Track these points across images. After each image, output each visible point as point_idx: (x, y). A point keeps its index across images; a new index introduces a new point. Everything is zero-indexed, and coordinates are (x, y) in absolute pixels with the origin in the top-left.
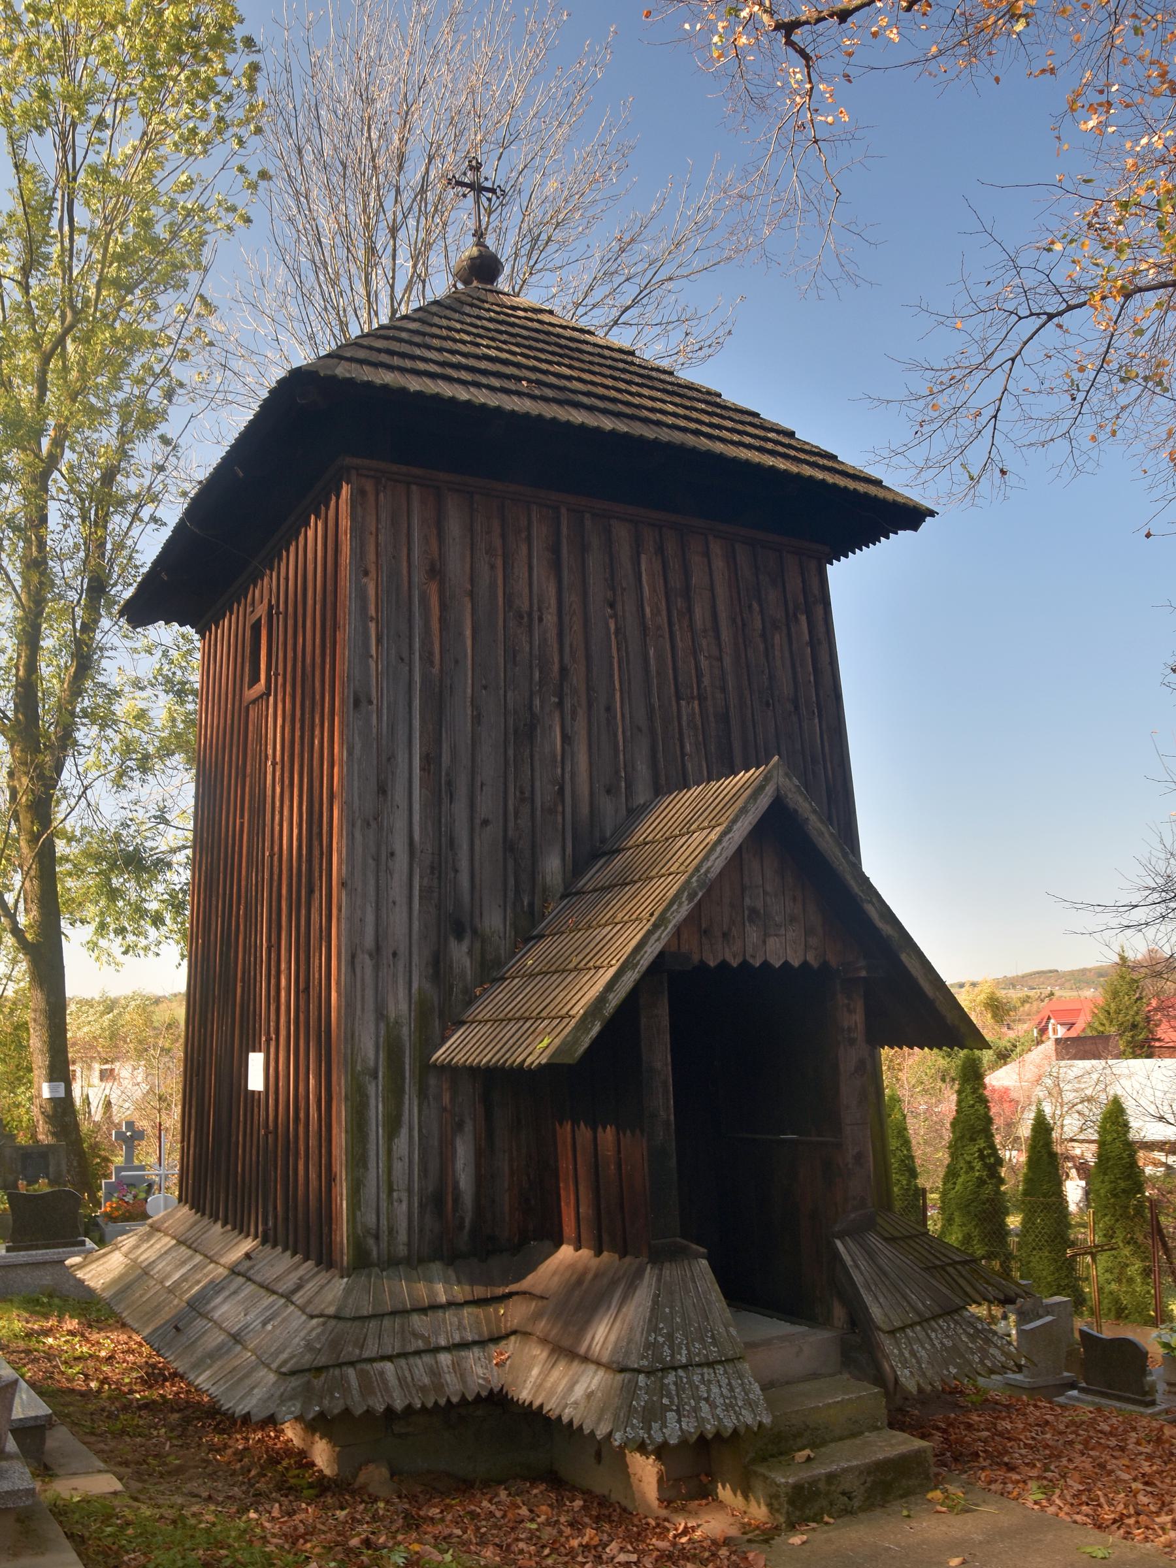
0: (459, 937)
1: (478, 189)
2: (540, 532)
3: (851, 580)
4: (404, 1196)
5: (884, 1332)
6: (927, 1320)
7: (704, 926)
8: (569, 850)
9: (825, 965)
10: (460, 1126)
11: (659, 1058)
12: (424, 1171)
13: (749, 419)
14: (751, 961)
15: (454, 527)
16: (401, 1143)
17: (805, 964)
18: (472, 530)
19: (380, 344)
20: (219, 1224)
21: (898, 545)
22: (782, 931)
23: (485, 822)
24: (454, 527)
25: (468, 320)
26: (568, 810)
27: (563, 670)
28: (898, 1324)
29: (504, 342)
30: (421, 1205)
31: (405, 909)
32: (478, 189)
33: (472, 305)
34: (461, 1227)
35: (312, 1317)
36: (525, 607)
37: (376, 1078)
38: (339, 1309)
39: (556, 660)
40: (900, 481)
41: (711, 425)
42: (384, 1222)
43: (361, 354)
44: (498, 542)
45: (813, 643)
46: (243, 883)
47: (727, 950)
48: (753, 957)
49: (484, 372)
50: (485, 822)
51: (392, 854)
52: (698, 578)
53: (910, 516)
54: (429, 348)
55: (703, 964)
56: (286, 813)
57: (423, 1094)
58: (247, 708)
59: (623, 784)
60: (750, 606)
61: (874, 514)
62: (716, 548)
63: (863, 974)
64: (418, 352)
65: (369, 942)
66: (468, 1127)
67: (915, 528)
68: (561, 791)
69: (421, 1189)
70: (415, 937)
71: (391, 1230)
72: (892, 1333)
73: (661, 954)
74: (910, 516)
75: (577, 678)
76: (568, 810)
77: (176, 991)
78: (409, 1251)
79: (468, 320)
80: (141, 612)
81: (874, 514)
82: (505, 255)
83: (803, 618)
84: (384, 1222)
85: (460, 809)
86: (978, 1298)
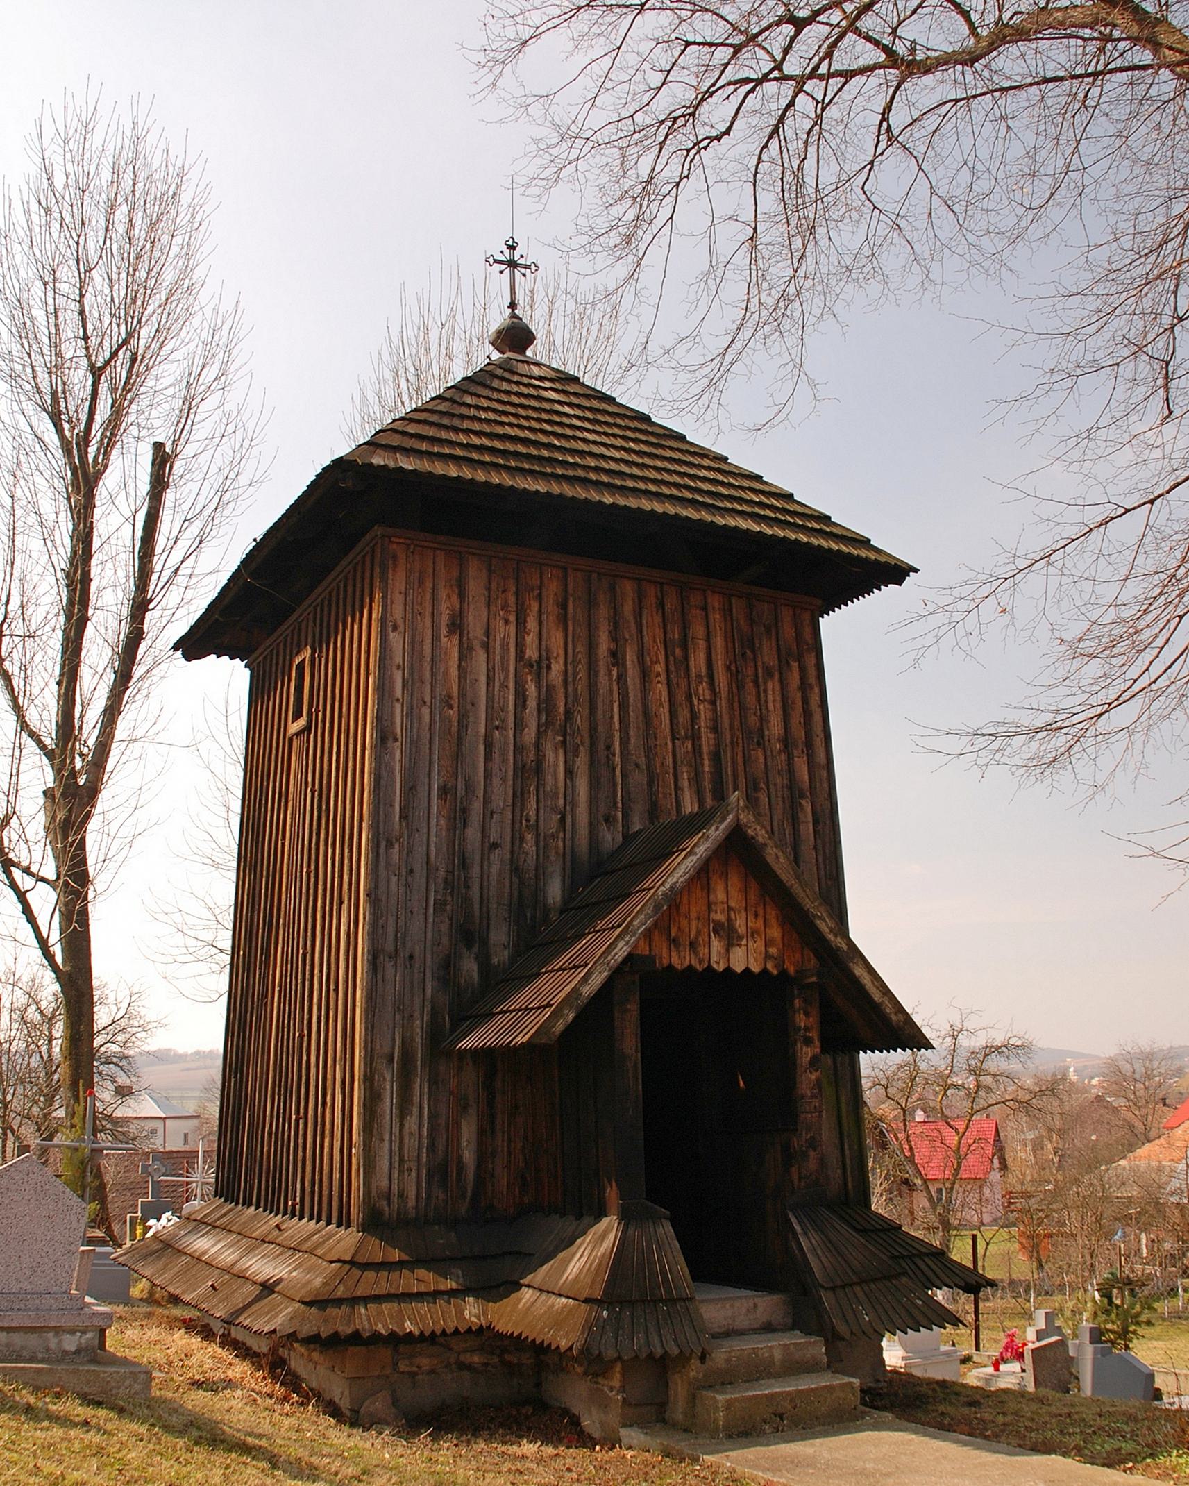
0: (469, 946)
1: (512, 264)
2: (552, 588)
3: (842, 630)
4: (413, 1165)
5: (826, 1289)
6: (865, 1282)
7: (673, 935)
8: (568, 872)
9: (783, 973)
10: (465, 1108)
11: (629, 1043)
12: (432, 1147)
13: (746, 483)
14: (715, 966)
15: (475, 587)
16: (411, 1123)
17: (765, 971)
18: (489, 589)
19: (412, 429)
20: (253, 1208)
21: (882, 601)
22: (744, 942)
23: (495, 846)
24: (475, 587)
25: (495, 396)
26: (568, 835)
27: (568, 713)
28: (839, 1283)
29: (527, 418)
30: (428, 1175)
31: (422, 917)
32: (512, 264)
33: (503, 379)
34: (464, 1195)
35: (331, 1262)
36: (535, 657)
37: (391, 1060)
38: (353, 1256)
39: (562, 704)
40: (889, 541)
41: (709, 493)
42: (395, 1187)
43: (396, 440)
44: (512, 600)
45: (804, 687)
46: (283, 897)
47: (674, 954)
48: (718, 963)
49: (504, 453)
50: (495, 846)
51: (412, 871)
52: (698, 630)
53: (896, 572)
54: (457, 430)
55: (670, 967)
56: (322, 836)
57: (434, 1081)
58: (291, 740)
59: (620, 814)
60: (744, 655)
61: (863, 571)
62: (715, 602)
63: (814, 979)
64: (444, 435)
65: (390, 947)
66: (472, 1111)
67: (899, 582)
68: (563, 820)
69: (429, 1161)
70: (429, 943)
71: (401, 1195)
72: (833, 1289)
73: (629, 958)
74: (896, 572)
75: (580, 721)
76: (568, 835)
77: (206, 1048)
78: (417, 1213)
79: (495, 396)
80: (194, 645)
81: (863, 571)
82: (538, 329)
83: (795, 665)
84: (395, 1187)
85: (472, 834)
86: (939, 1283)
